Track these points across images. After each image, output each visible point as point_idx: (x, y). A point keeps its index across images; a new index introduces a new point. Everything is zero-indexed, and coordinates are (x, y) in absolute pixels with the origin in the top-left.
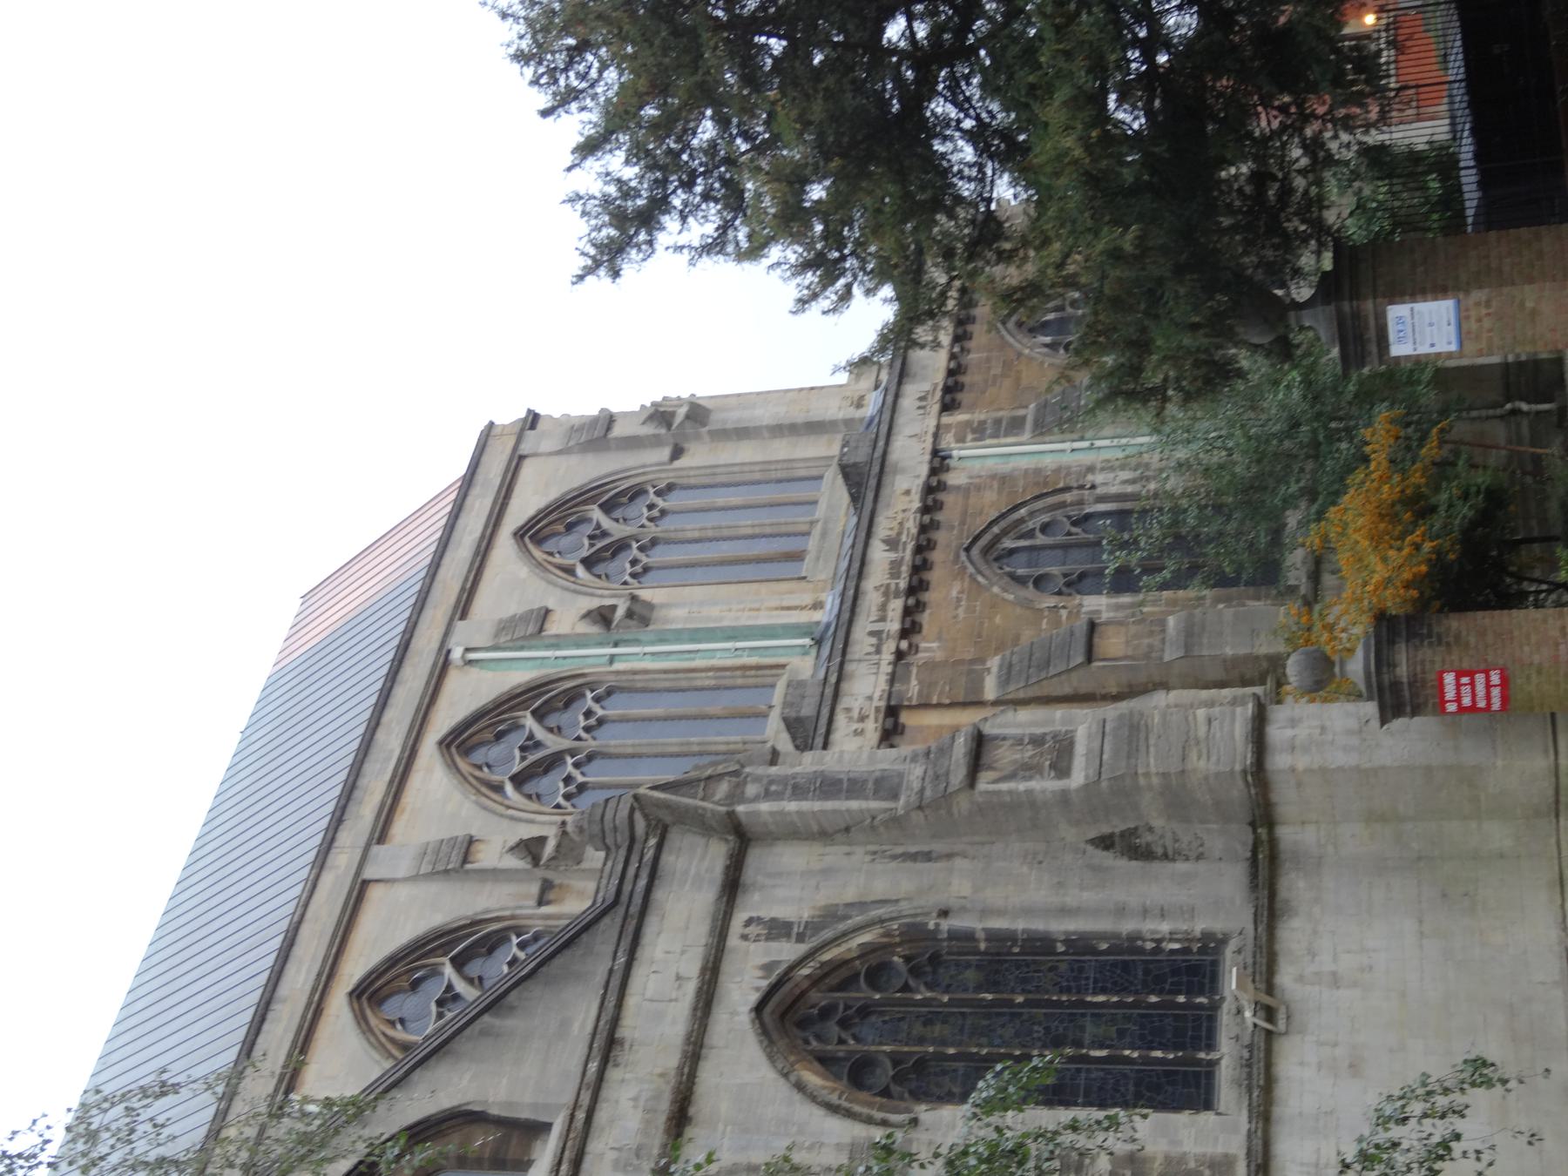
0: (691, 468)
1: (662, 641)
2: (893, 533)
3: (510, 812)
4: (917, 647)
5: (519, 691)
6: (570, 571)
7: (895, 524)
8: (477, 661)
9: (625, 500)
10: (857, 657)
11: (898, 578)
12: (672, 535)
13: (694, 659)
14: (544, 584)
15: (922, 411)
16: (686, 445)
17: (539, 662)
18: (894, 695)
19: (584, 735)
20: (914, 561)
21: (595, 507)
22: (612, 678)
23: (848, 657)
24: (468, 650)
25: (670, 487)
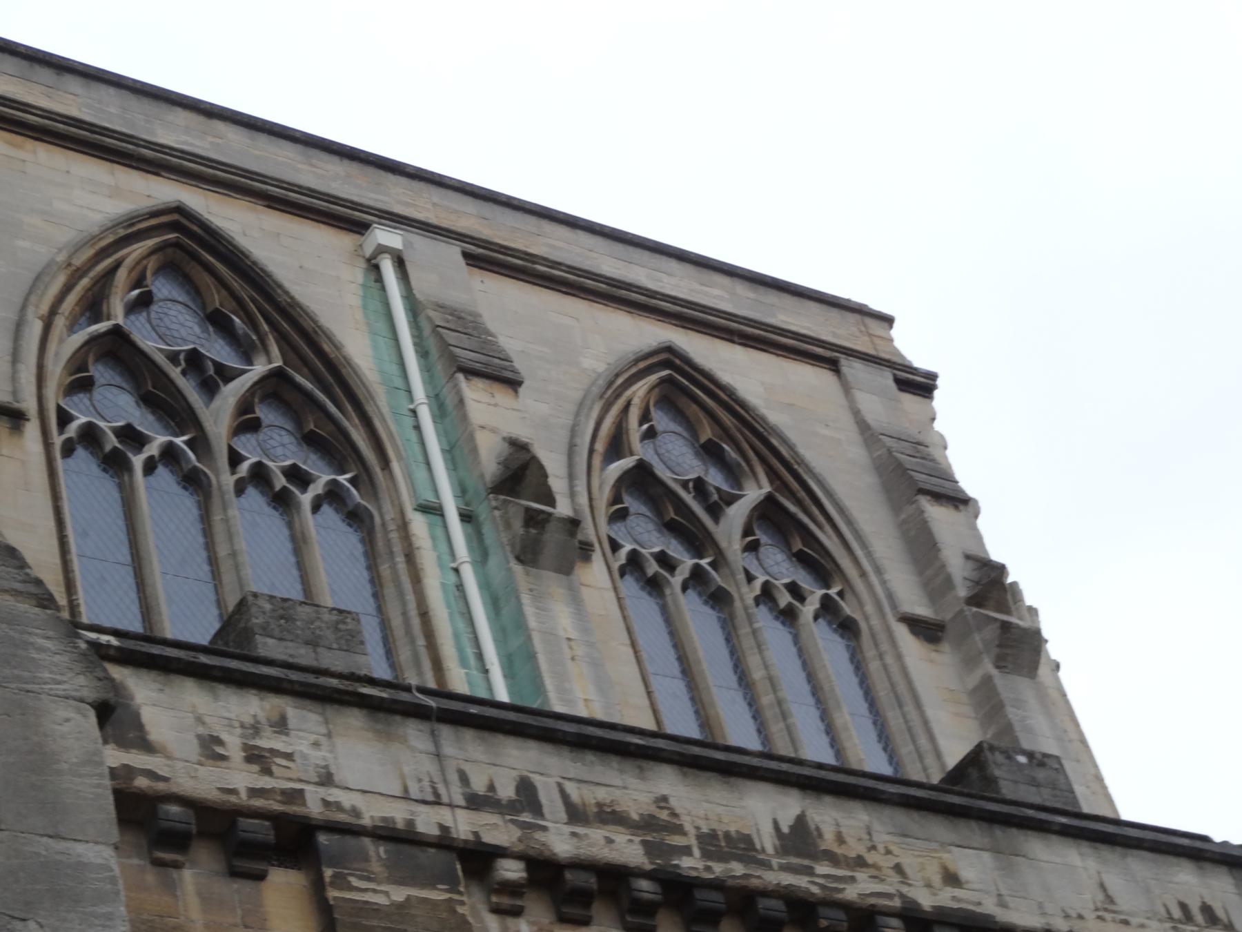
0: (899, 657)
1: (494, 604)
2: (828, 841)
3: (36, 327)
4: (516, 912)
5: (326, 347)
6: (617, 447)
7: (855, 848)
8: (379, 279)
9: (798, 545)
10: (449, 749)
11: (706, 855)
12: (744, 630)
13: (464, 663)
14: (578, 395)
15: (1177, 913)
16: (946, 647)
17: (399, 382)
18: (350, 841)
19: (244, 468)
20: (765, 893)
21: (767, 488)
22: (390, 514)
23: (446, 731)
24: (400, 263)
25: (847, 628)
